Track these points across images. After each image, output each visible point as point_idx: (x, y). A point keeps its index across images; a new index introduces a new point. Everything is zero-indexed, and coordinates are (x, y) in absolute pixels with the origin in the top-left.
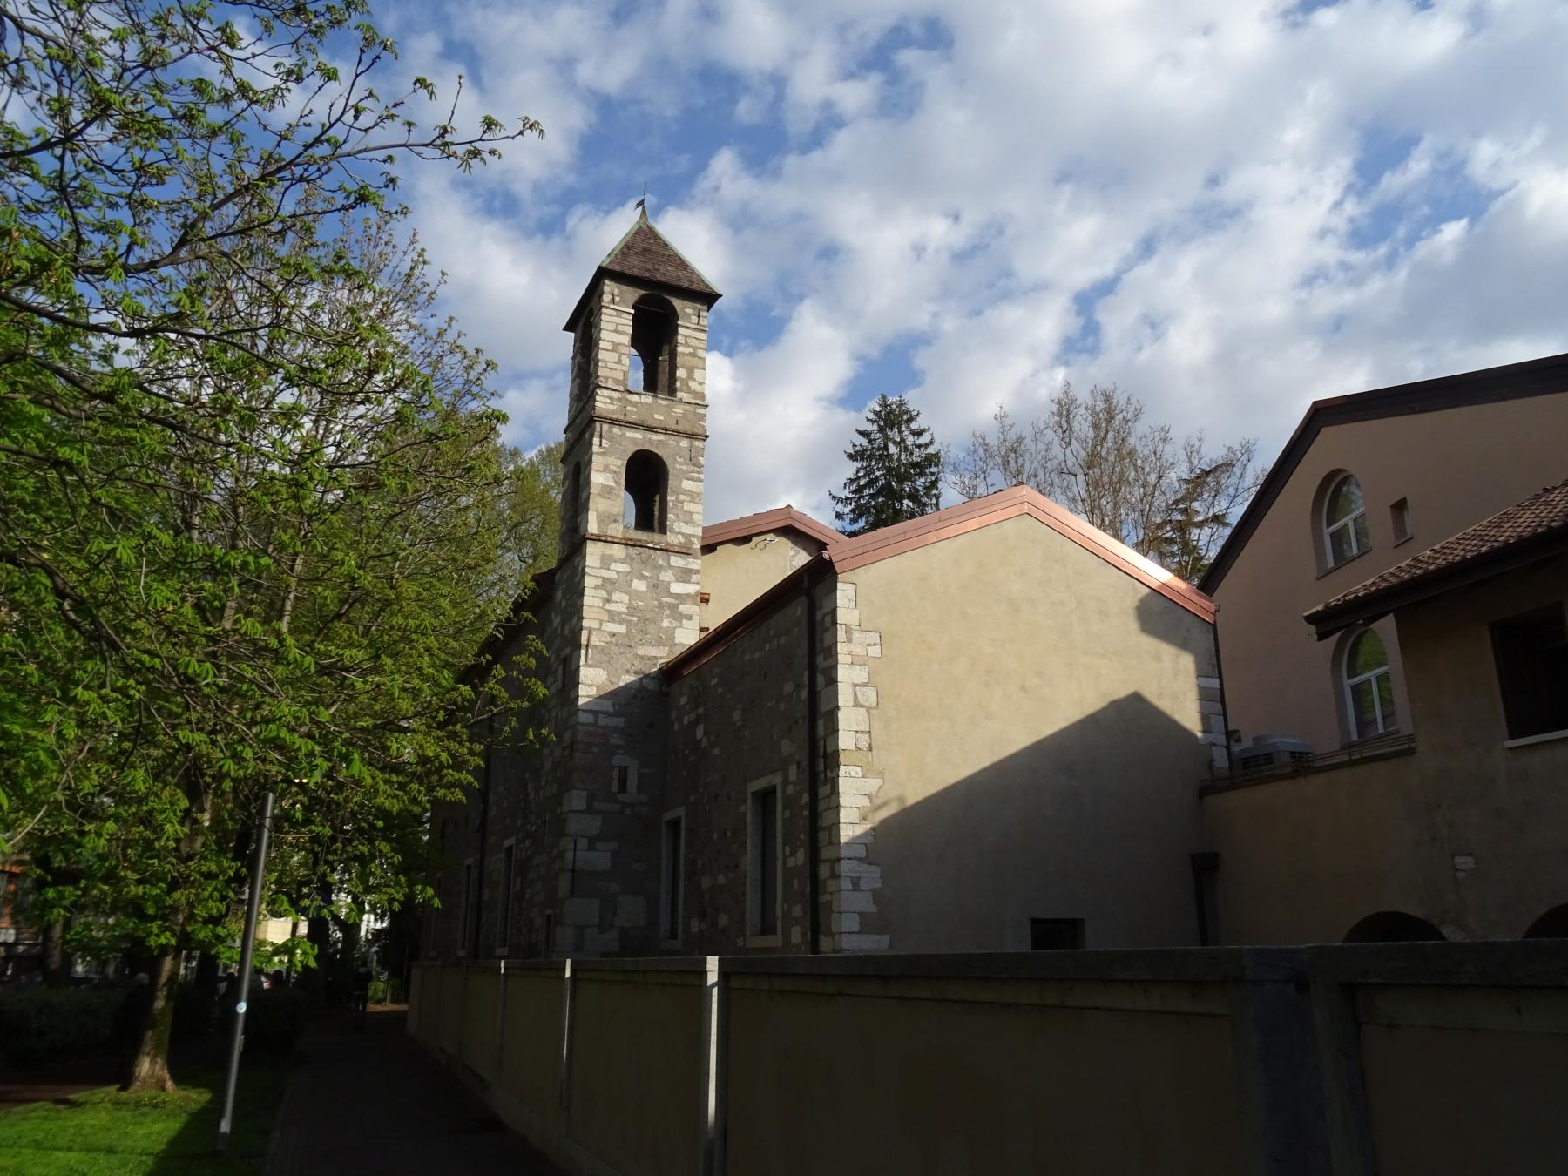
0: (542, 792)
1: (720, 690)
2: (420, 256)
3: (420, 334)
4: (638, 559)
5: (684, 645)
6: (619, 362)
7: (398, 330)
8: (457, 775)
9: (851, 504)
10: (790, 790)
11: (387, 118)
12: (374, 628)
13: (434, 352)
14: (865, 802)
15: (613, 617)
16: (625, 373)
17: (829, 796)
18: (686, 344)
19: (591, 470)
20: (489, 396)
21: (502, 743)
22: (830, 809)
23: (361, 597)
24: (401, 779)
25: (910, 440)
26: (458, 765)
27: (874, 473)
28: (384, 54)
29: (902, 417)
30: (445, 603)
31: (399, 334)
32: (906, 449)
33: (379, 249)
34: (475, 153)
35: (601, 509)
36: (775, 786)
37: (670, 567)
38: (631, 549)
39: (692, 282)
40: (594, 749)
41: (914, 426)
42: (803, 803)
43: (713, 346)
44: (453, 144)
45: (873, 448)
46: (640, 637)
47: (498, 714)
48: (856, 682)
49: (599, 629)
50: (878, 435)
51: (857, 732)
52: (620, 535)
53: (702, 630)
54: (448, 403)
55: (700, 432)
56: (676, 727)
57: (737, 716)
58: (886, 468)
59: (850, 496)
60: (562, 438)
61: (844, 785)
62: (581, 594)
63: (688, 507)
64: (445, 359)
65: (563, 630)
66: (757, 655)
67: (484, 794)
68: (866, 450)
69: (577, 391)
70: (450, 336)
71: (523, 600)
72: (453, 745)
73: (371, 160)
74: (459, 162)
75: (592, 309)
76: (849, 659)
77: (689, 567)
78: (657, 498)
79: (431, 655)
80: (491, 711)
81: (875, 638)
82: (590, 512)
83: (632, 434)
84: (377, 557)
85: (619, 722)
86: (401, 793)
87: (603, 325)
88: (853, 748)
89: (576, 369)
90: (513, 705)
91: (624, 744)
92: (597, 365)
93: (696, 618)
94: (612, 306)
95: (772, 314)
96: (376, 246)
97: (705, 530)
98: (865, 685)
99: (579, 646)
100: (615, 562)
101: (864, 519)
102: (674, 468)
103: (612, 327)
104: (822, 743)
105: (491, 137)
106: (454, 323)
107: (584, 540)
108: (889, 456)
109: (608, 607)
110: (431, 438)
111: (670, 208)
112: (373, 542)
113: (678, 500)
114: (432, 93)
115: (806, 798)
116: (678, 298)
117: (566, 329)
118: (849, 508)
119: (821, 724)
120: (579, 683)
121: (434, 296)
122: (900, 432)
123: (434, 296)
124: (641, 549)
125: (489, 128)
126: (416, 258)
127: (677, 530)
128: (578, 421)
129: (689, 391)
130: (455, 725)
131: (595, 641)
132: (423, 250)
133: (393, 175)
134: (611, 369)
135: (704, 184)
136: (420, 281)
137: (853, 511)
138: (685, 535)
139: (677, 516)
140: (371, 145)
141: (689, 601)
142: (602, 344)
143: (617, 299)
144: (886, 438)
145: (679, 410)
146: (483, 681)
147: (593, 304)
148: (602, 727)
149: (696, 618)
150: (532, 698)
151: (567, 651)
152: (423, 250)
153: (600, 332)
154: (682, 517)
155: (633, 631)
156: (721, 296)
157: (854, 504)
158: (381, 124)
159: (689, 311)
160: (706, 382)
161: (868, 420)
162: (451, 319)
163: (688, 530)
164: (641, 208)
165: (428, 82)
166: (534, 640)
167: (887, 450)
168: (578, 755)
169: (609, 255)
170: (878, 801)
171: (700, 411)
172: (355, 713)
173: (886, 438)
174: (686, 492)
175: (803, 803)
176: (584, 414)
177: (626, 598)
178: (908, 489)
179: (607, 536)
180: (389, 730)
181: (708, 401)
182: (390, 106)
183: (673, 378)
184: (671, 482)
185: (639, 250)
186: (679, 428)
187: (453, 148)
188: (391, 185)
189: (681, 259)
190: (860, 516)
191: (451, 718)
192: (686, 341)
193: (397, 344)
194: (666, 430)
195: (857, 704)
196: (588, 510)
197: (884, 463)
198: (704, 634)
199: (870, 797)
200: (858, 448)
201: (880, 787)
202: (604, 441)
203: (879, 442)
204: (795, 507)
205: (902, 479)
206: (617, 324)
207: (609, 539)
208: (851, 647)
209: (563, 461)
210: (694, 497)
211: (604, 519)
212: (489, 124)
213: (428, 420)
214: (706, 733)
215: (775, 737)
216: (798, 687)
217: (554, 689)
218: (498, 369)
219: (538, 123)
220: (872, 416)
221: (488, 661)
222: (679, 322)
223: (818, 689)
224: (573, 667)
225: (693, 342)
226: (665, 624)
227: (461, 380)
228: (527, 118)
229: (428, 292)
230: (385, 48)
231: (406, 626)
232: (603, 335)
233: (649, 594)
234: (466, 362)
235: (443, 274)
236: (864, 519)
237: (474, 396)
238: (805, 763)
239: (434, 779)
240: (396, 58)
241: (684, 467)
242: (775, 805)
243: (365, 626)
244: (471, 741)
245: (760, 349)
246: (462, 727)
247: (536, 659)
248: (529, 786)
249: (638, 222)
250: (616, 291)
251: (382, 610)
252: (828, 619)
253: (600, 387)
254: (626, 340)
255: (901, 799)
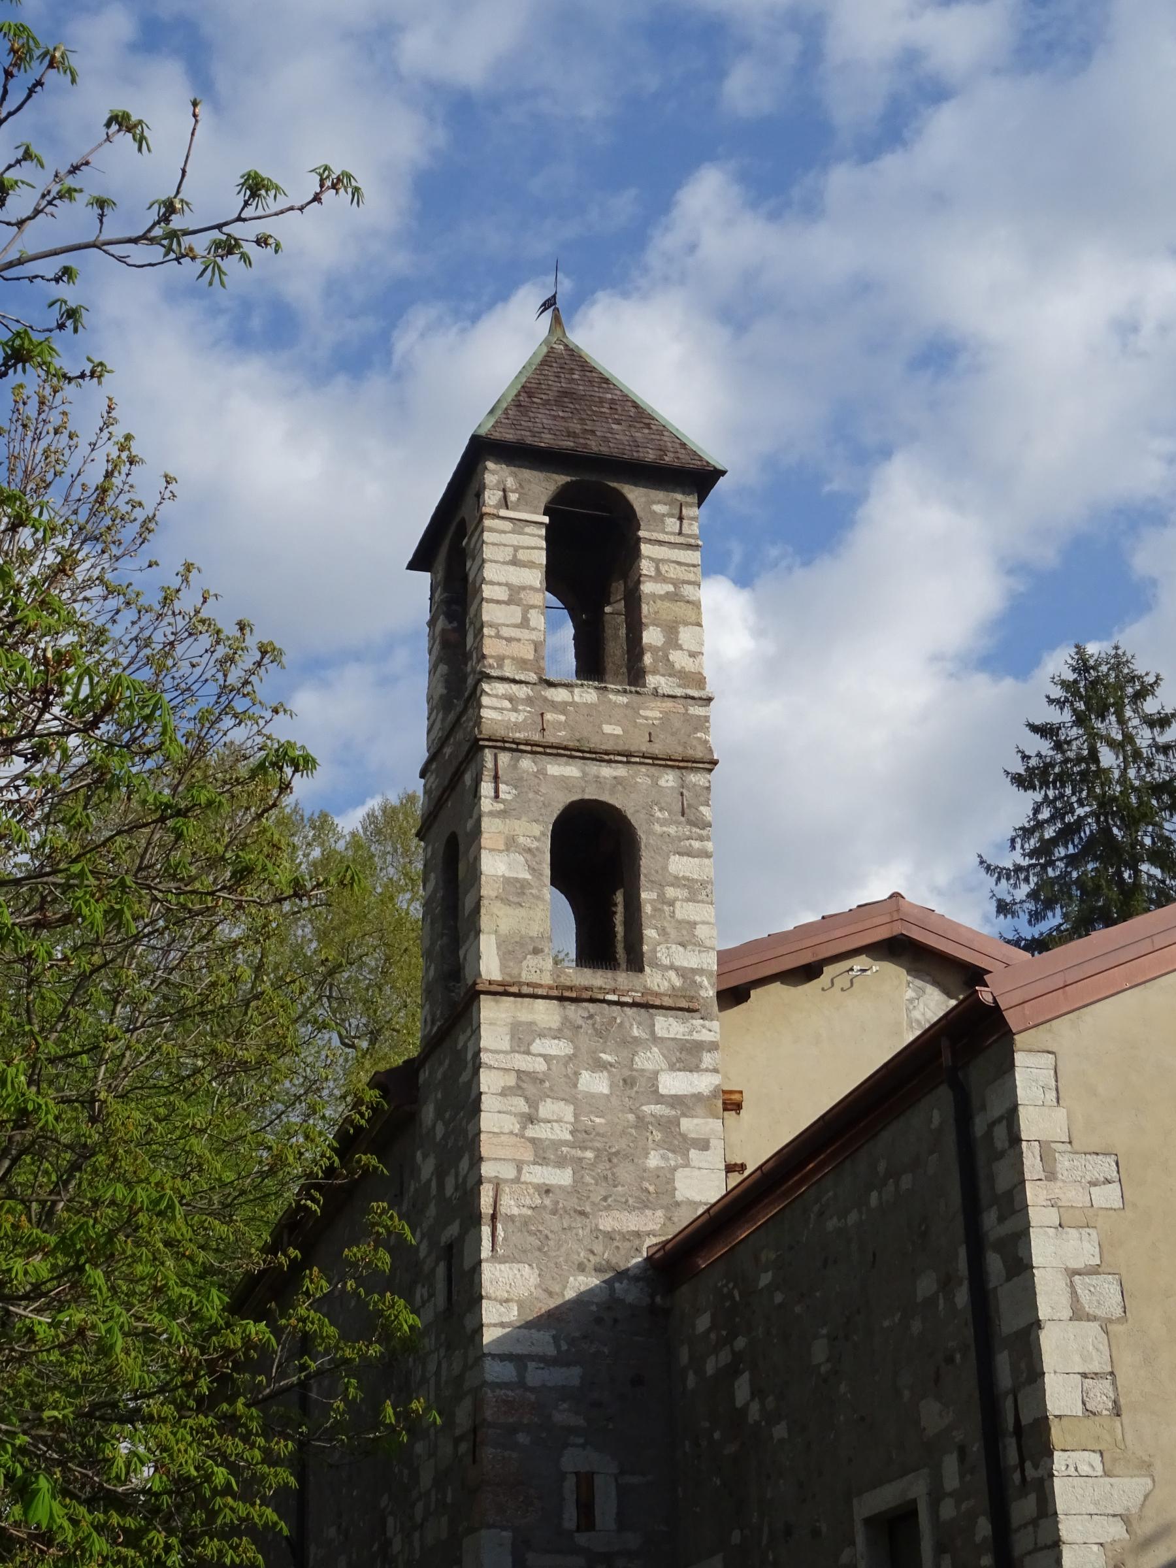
0: (417, 1535)
1: (779, 1298)
2: (121, 450)
3: (128, 604)
4: (586, 1027)
5: (695, 1204)
6: (525, 624)
7: (86, 599)
8: (242, 1509)
9: (1027, 880)
10: (948, 1510)
11: (60, 196)
12: (61, 1205)
13: (158, 637)
14: (1116, 1530)
15: (543, 1153)
16: (537, 646)
17: (1034, 1522)
18: (659, 577)
19: (480, 848)
20: (268, 714)
21: (330, 1435)
22: (1037, 1549)
23: (33, 1143)
24: (130, 1522)
25: (1144, 737)
26: (249, 1489)
27: (1072, 811)
28: (52, 77)
29: (1122, 689)
30: (199, 1145)
31: (87, 606)
32: (1137, 754)
33: (43, 444)
34: (229, 247)
35: (504, 928)
36: (914, 1501)
37: (655, 1039)
38: (571, 1008)
39: (663, 451)
40: (522, 1438)
41: (1150, 706)
42: (978, 1539)
43: (713, 567)
44: (186, 233)
45: (1067, 760)
46: (603, 1193)
47: (320, 1372)
48: (1078, 1264)
49: (517, 1180)
50: (1074, 732)
51: (1084, 1375)
52: (547, 979)
53: (730, 1168)
54: (188, 736)
55: (699, 754)
56: (691, 1380)
57: (819, 1352)
58: (1096, 798)
59: (1025, 862)
60: (418, 786)
61: (1065, 1493)
62: (475, 1109)
63: (686, 911)
64: (180, 649)
65: (441, 1186)
66: (853, 1217)
67: (297, 1546)
68: (1052, 765)
69: (441, 690)
70: (187, 602)
71: (359, 1129)
72: (232, 1445)
73: (32, 279)
74: (198, 266)
75: (463, 521)
76: (1052, 1216)
77: (696, 1036)
78: (619, 897)
79: (179, 1256)
80: (304, 1367)
81: (1106, 1167)
82: (482, 937)
83: (557, 769)
84: (61, 1059)
85: (572, 1376)
86: (131, 1553)
87: (488, 552)
88: (1078, 1410)
89: (437, 646)
90: (348, 1353)
91: (581, 1422)
92: (479, 633)
93: (716, 1144)
94: (503, 512)
95: (827, 488)
96: (37, 438)
97: (723, 956)
98: (1093, 1271)
99: (475, 1219)
100: (541, 1035)
101: (1058, 911)
102: (650, 832)
103: (506, 554)
104: (1009, 1403)
105: (260, 212)
106: (194, 573)
107: (473, 995)
108: (1104, 773)
109: (531, 1132)
110: (166, 813)
111: (600, 295)
112: (53, 1029)
113: (662, 899)
114: (141, 140)
115: (984, 1528)
116: (636, 485)
117: (412, 566)
118: (1024, 890)
119: (1003, 1361)
120: (481, 1298)
121: (152, 526)
122: (1122, 721)
123: (152, 526)
124: (591, 1007)
125: (254, 195)
126: (114, 453)
127: (666, 962)
128: (448, 751)
129: (671, 671)
130: (232, 1401)
131: (509, 1205)
132: (128, 437)
133: (72, 304)
134: (509, 640)
135: (667, 241)
136: (124, 497)
137: (1033, 895)
138: (682, 972)
139: (663, 932)
140: (31, 251)
141: (700, 1110)
142: (487, 591)
143: (513, 497)
144: (1093, 736)
145: (652, 712)
146: (286, 1305)
147: (465, 512)
148: (532, 1390)
149: (716, 1144)
150: (387, 1336)
151: (453, 1230)
152: (128, 437)
153: (481, 567)
154: (673, 933)
155: (588, 1179)
156: (723, 473)
157: (1033, 880)
158: (49, 209)
159: (659, 509)
160: (705, 650)
161: (1051, 701)
162: (188, 567)
163: (688, 959)
164: (548, 314)
165: (134, 119)
166: (384, 1211)
167: (1097, 761)
168: (488, 1453)
169: (492, 412)
170: (1145, 1528)
171: (696, 710)
172: (28, 1384)
173: (1093, 736)
174: (677, 882)
175: (978, 1539)
176: (459, 735)
177: (568, 1112)
178: (1148, 841)
179: (520, 984)
180: (101, 1418)
181: (710, 689)
182: (63, 172)
183: (635, 648)
184: (647, 862)
185: (552, 395)
186: (657, 749)
187: (186, 241)
188: (69, 323)
189: (636, 406)
190: (1049, 904)
191: (225, 1389)
192: (658, 569)
193: (85, 626)
194: (628, 755)
195: (1078, 1314)
196: (478, 932)
197: (1091, 790)
198: (736, 1179)
199: (1125, 1519)
200: (1033, 762)
201: (1146, 1497)
202: (502, 787)
203: (1075, 749)
204: (910, 897)
205: (1134, 819)
206: (516, 548)
207: (525, 990)
208: (1056, 1189)
209: (420, 835)
210: (695, 889)
211: (512, 949)
212: (255, 186)
213: (151, 772)
214: (757, 1392)
215: (907, 1394)
216: (947, 1283)
217: (429, 1313)
218: (284, 659)
219: (349, 176)
220: (1058, 693)
221: (293, 1262)
222: (641, 534)
223: (991, 1285)
224: (467, 1265)
225: (672, 572)
226: (654, 1160)
227: (212, 689)
228: (326, 168)
229: (141, 519)
230: (51, 65)
231: (134, 1201)
232: (489, 572)
233: (613, 1099)
234: (221, 651)
235: (169, 480)
236: (1058, 911)
237: (239, 718)
238: (976, 1448)
239: (198, 1517)
240: (73, 81)
241: (672, 830)
242: (480, 1240)
243: (43, 1203)
244: (267, 1433)
245: (806, 563)
246: (248, 1405)
247: (390, 1251)
248: (390, 1521)
249: (546, 341)
250: (510, 482)
251: (75, 1167)
252: (1000, 1132)
253: (489, 677)
254: (536, 578)
255: (515, 1002)
